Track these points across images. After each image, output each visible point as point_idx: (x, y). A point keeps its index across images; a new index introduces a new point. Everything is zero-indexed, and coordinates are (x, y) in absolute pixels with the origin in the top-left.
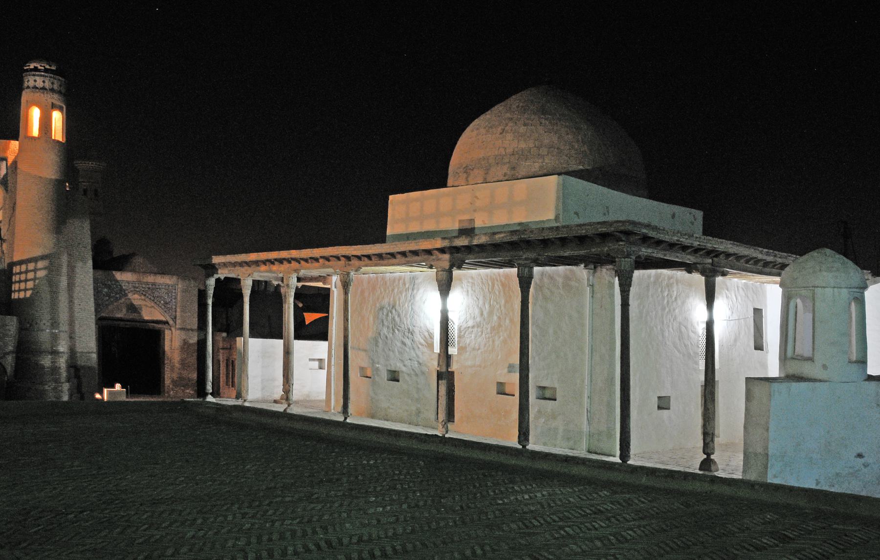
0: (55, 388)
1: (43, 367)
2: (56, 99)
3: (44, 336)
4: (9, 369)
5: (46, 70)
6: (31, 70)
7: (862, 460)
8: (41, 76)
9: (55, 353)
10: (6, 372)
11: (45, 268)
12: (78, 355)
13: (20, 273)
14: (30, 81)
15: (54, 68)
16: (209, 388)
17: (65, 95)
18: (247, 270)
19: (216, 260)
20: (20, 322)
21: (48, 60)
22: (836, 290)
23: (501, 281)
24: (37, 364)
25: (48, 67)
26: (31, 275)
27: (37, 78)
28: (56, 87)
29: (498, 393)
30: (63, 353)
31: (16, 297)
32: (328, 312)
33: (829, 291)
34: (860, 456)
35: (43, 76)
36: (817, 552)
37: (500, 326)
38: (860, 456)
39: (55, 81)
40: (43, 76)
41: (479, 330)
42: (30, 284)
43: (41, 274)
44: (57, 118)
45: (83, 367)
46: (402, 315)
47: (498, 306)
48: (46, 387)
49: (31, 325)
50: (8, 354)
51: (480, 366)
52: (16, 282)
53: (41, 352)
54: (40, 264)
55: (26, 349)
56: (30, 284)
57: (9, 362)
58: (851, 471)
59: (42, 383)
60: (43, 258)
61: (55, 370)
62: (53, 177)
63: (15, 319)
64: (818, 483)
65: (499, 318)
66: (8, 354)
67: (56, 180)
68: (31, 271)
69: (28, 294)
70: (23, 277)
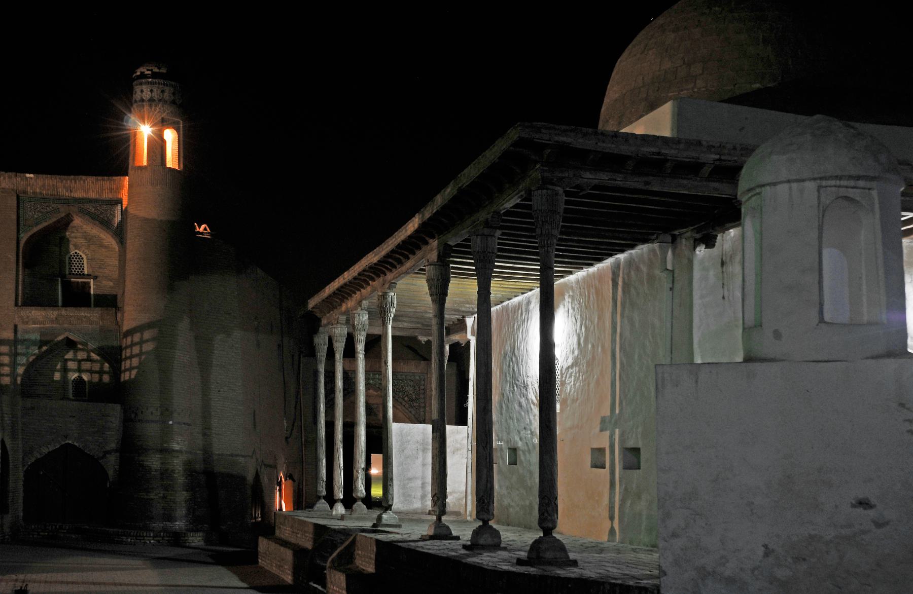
3: (150, 431)
4: (111, 473)
5: (154, 75)
6: (139, 77)
7: (871, 513)
9: (165, 451)
11: (153, 339)
12: (215, 457)
13: (133, 344)
15: (164, 71)
22: (795, 185)
26: (136, 350)
27: (144, 87)
28: (167, 96)
29: (592, 467)
30: (180, 451)
31: (127, 378)
32: (66, 304)
33: (783, 189)
34: (864, 504)
35: (151, 83)
36: (127, 543)
38: (864, 504)
39: (167, 89)
42: (135, 362)
43: (149, 347)
44: (170, 136)
48: (152, 496)
49: (136, 414)
50: (109, 452)
54: (147, 335)
55: (131, 446)
56: (135, 362)
57: (111, 464)
58: (845, 532)
60: (149, 326)
61: (166, 474)
63: (118, 407)
64: (451, 493)
66: (109, 452)
69: (134, 372)
70: (136, 350)
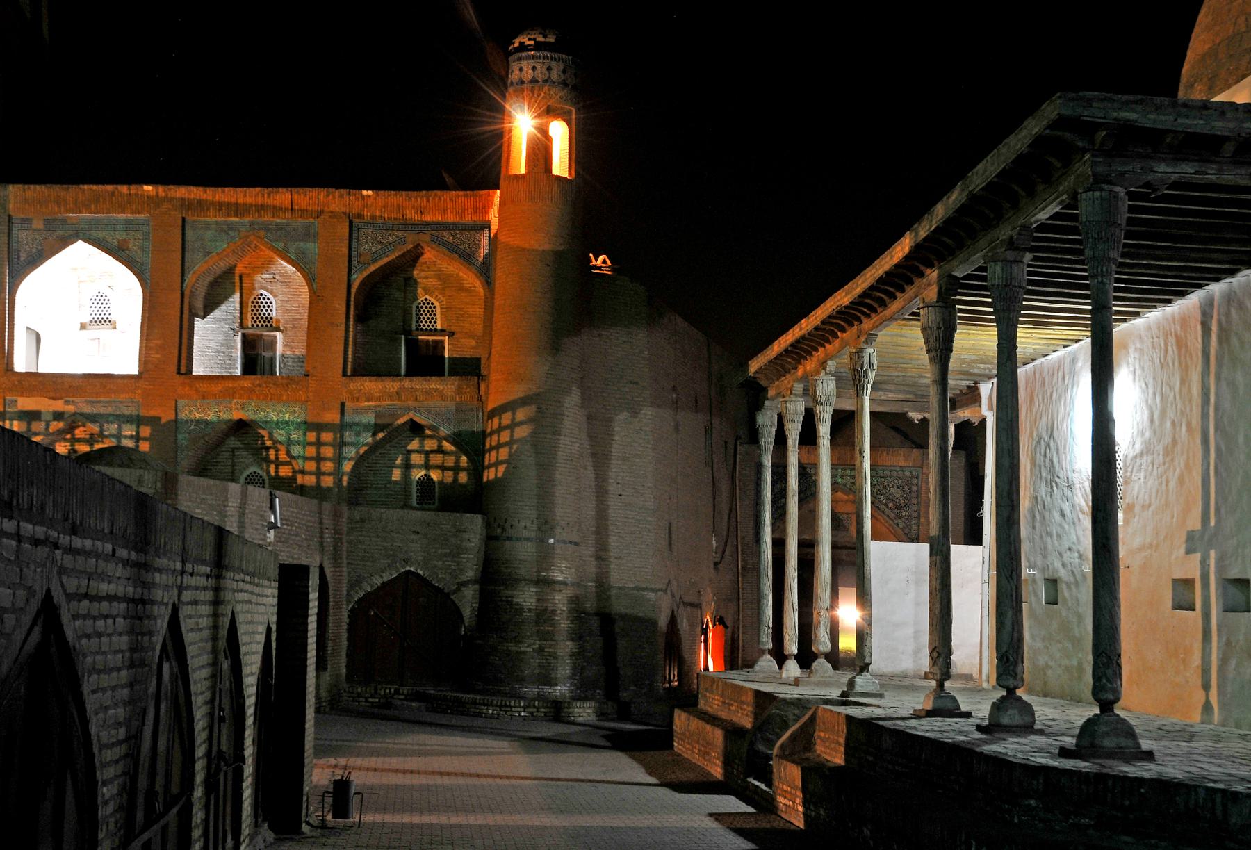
0: (541, 650)
1: (520, 610)
2: (557, 95)
3: (523, 552)
5: (538, 46)
8: (530, 57)
9: (544, 583)
10: (463, 622)
11: (530, 421)
12: (614, 592)
14: (522, 69)
15: (551, 39)
16: (792, 647)
17: (574, 88)
18: (414, 327)
19: (754, 366)
20: (488, 525)
21: (544, 28)
23: (1176, 336)
24: (510, 603)
25: (540, 39)
28: (555, 75)
29: (1175, 608)
35: (533, 57)
37: (1174, 442)
39: (554, 64)
40: (533, 57)
41: (1150, 458)
43: (522, 432)
44: (559, 132)
45: (624, 617)
46: (1061, 449)
47: (1172, 396)
49: (504, 529)
50: (464, 584)
51: (1151, 545)
52: (492, 448)
53: (518, 581)
54: (521, 414)
57: (468, 601)
59: (517, 640)
60: (524, 401)
61: (544, 615)
62: (547, 247)
63: (478, 519)
65: (1173, 423)
66: (464, 584)
67: (558, 255)
68: (507, 427)
69: (502, 468)
